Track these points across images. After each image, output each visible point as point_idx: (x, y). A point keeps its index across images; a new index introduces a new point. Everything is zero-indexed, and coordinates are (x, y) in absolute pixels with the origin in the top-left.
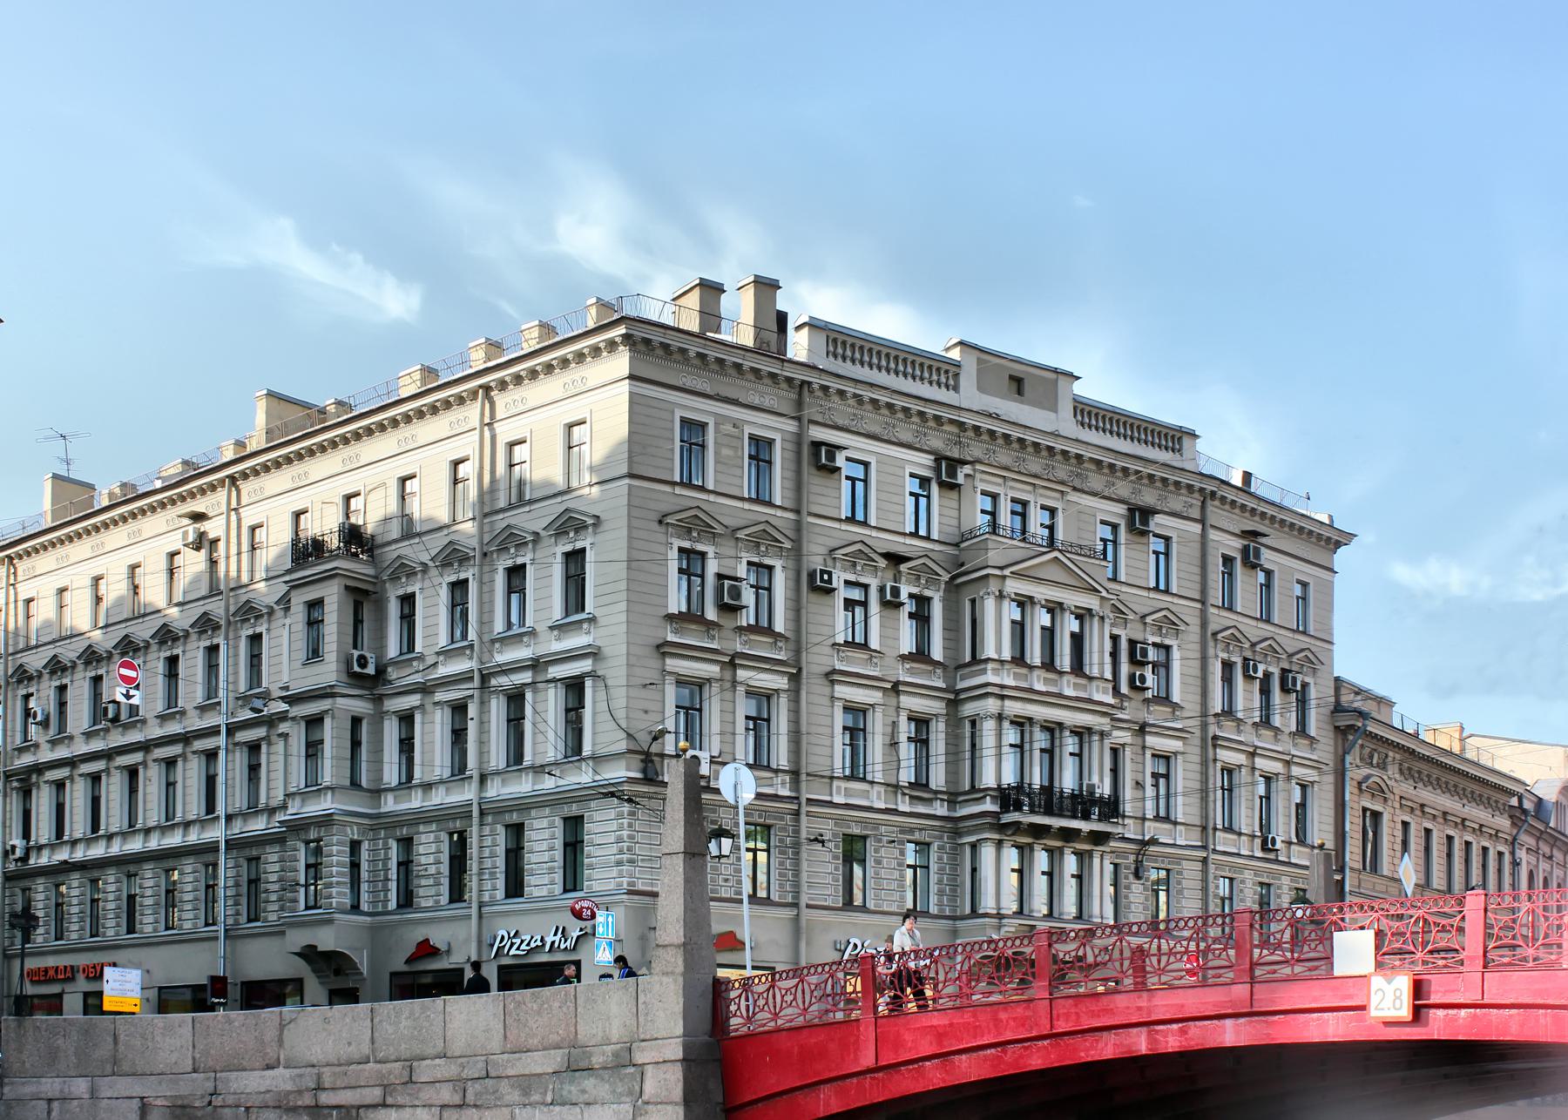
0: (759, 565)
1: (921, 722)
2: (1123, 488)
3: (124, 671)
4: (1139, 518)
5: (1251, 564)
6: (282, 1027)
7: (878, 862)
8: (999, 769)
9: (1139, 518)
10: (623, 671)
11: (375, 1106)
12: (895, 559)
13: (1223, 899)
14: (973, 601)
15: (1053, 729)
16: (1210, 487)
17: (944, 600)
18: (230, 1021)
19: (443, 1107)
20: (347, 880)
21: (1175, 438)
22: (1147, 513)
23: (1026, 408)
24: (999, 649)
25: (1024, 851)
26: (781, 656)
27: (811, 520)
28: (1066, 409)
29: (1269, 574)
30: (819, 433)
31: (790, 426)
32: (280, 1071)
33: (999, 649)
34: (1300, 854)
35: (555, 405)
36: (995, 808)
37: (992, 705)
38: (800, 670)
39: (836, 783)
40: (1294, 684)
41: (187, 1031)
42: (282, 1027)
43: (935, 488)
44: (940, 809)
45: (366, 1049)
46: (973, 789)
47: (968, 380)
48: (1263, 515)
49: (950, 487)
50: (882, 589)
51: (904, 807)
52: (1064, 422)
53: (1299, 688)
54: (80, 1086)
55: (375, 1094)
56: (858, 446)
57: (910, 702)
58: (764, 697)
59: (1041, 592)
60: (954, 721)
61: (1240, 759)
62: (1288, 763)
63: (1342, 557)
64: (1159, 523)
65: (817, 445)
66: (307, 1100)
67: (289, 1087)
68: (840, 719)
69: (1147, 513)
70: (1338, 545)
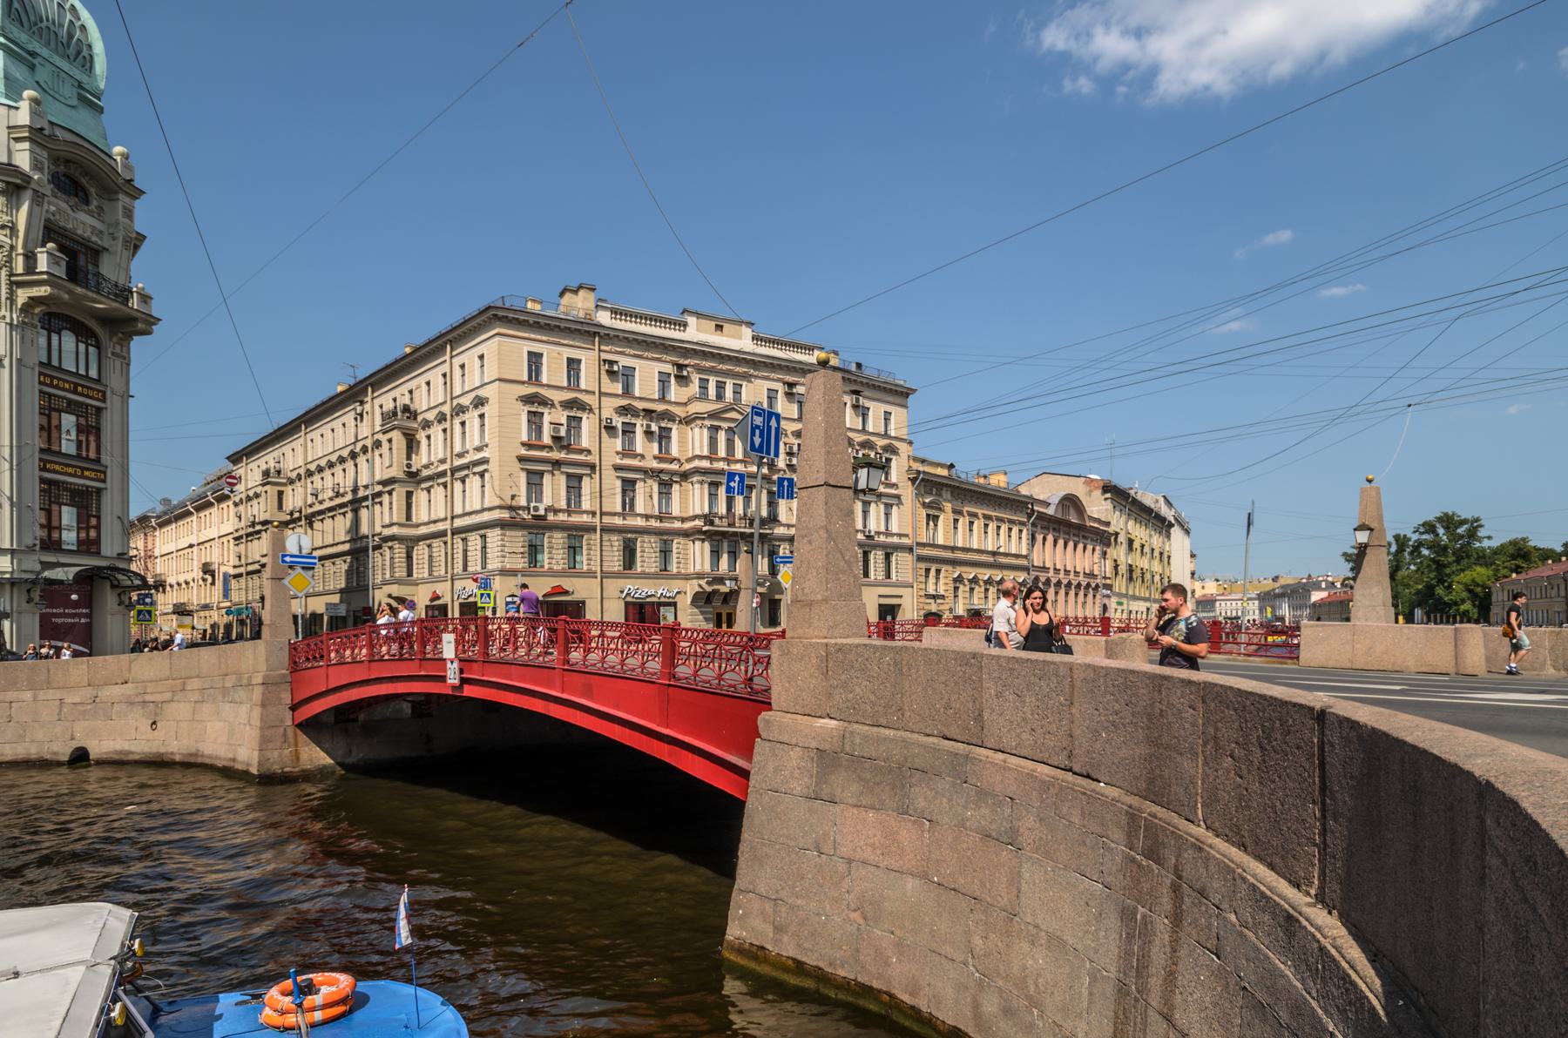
0: (535, 413)
3: (228, 480)
6: (130, 663)
7: (643, 551)
10: (497, 468)
11: (169, 702)
18: (105, 661)
19: (196, 702)
20: (405, 565)
23: (725, 338)
24: (702, 450)
32: (130, 685)
33: (702, 450)
35: (1332, 339)
41: (85, 666)
42: (130, 663)
43: (673, 379)
45: (168, 673)
48: (861, 382)
50: (642, 425)
54: (28, 695)
55: (168, 696)
56: (624, 361)
66: (140, 699)
67: (132, 693)
68: (619, 483)
69: (791, 385)
70: (907, 395)
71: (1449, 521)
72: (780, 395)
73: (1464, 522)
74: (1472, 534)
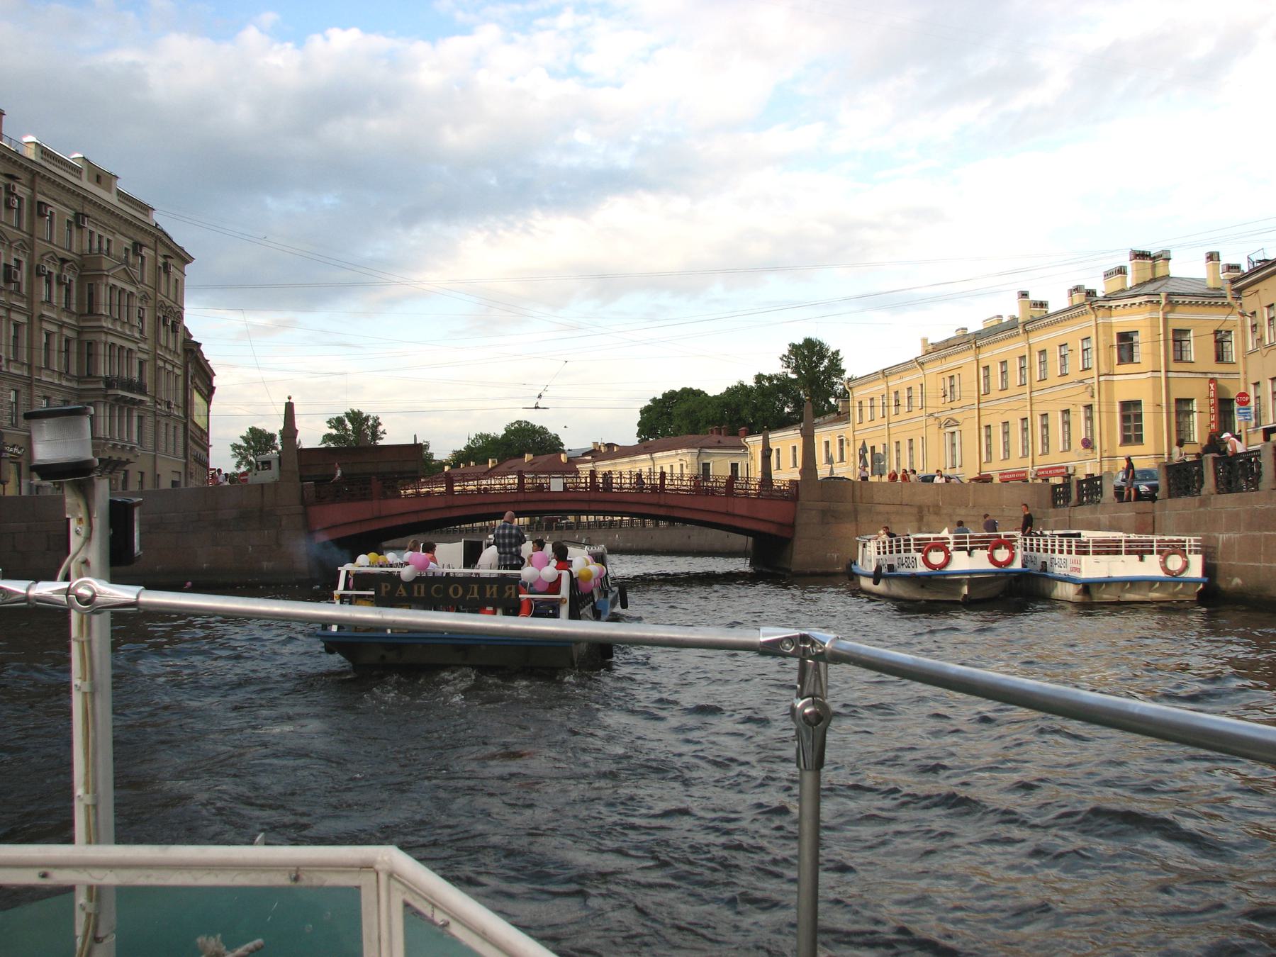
1: (68, 341)
2: (131, 232)
4: (137, 246)
5: (167, 272)
8: (103, 370)
9: (137, 246)
12: (64, 261)
13: (12, 403)
14: (90, 285)
15: (122, 348)
16: (160, 235)
17: (77, 282)
21: (146, 209)
22: (142, 246)
25: (121, 409)
26: (24, 306)
27: (37, 240)
28: (114, 192)
29: (143, 258)
30: (40, 198)
31: (28, 191)
34: (47, 376)
36: (103, 386)
37: (103, 337)
38: (33, 314)
39: (43, 371)
40: (65, 279)
44: (74, 385)
46: (89, 375)
47: (85, 174)
49: (80, 227)
51: (64, 383)
52: (112, 199)
53: (68, 282)
57: (66, 332)
58: (17, 326)
59: (120, 284)
60: (80, 342)
61: (54, 328)
62: (9, 310)
63: (188, 267)
64: (145, 251)
65: (40, 203)
70: (188, 262)
71: (356, 417)
72: (131, 253)
73: (367, 419)
74: (375, 435)
